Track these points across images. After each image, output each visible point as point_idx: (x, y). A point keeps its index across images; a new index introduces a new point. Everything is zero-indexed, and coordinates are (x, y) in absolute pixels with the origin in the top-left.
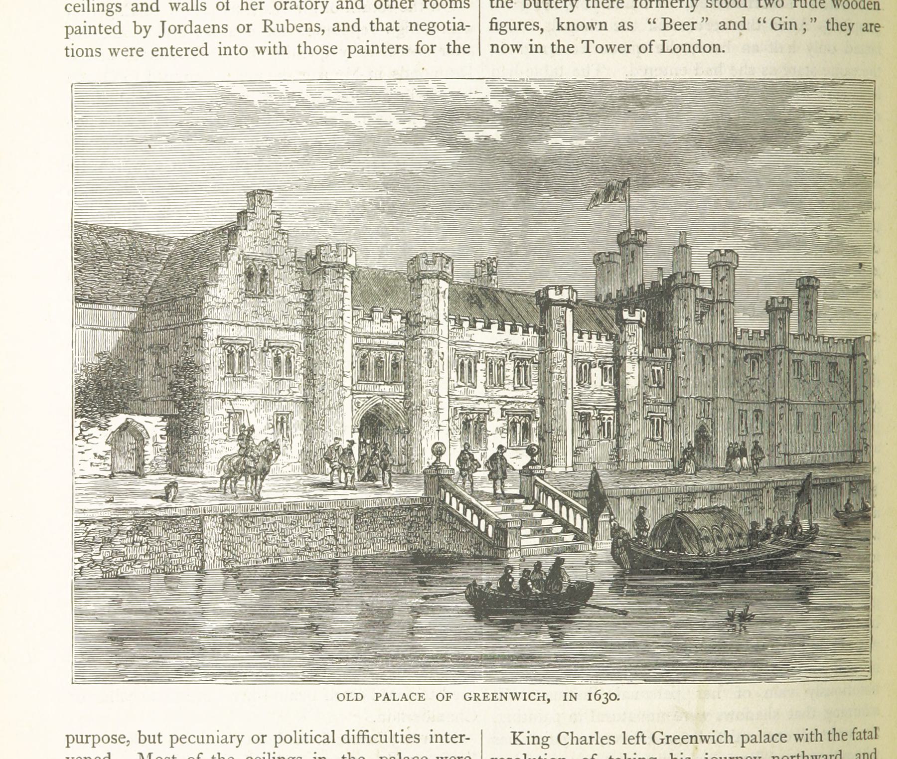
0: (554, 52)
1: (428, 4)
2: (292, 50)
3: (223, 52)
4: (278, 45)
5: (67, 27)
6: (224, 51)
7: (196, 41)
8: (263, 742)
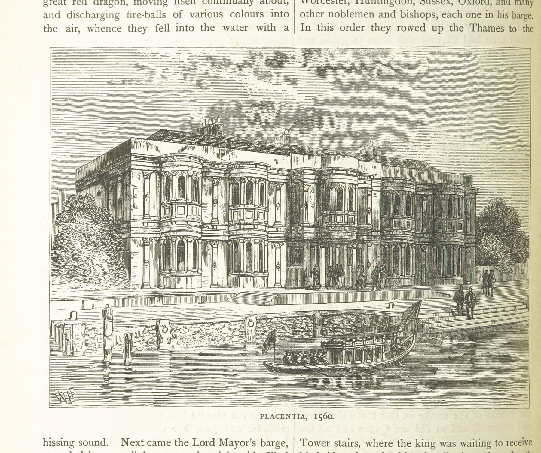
0: (511, 31)
1: (75, 2)
2: (314, 28)
3: (179, 29)
4: (270, 25)
5: (59, 17)
6: (180, 29)
7: (419, 22)
8: (180, 17)
